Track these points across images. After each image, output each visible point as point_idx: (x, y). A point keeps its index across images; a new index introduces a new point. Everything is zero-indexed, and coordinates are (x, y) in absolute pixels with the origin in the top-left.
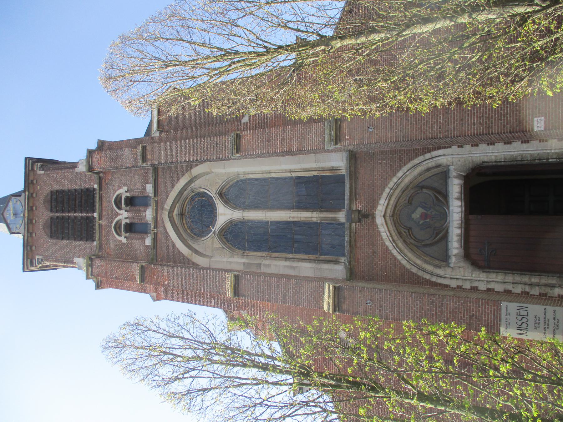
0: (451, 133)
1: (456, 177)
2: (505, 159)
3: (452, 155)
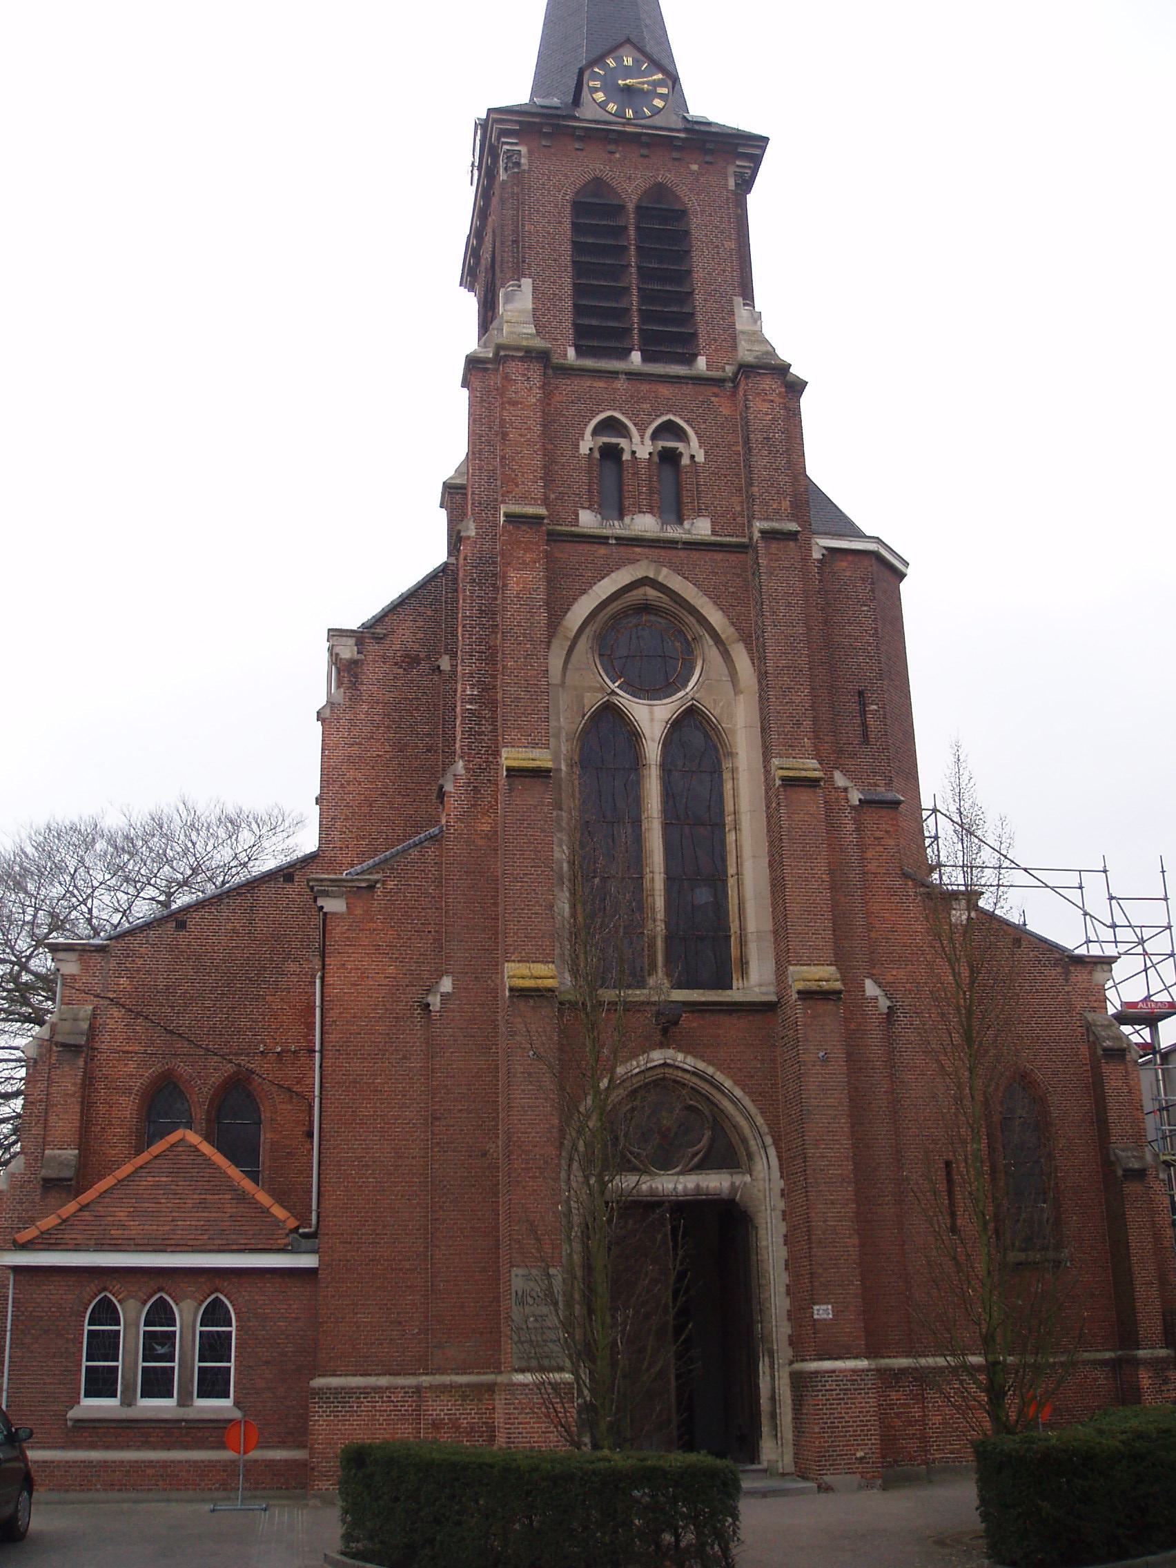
0: (812, 1187)
1: (733, 1184)
2: (762, 1261)
3: (770, 1180)
